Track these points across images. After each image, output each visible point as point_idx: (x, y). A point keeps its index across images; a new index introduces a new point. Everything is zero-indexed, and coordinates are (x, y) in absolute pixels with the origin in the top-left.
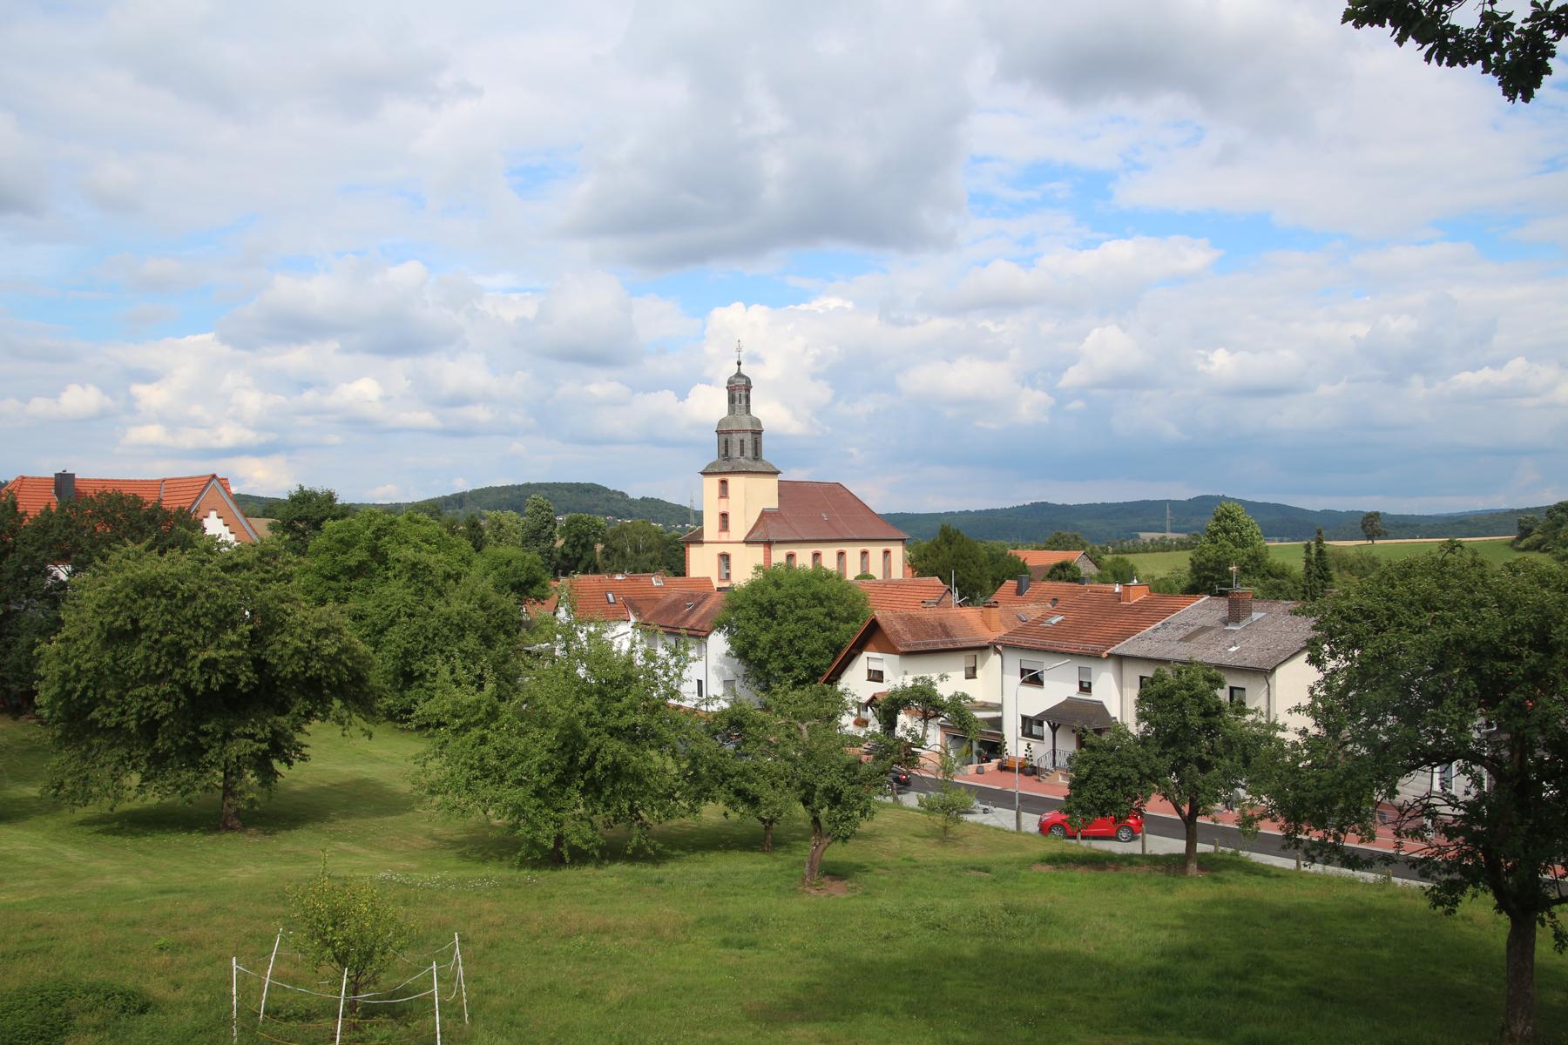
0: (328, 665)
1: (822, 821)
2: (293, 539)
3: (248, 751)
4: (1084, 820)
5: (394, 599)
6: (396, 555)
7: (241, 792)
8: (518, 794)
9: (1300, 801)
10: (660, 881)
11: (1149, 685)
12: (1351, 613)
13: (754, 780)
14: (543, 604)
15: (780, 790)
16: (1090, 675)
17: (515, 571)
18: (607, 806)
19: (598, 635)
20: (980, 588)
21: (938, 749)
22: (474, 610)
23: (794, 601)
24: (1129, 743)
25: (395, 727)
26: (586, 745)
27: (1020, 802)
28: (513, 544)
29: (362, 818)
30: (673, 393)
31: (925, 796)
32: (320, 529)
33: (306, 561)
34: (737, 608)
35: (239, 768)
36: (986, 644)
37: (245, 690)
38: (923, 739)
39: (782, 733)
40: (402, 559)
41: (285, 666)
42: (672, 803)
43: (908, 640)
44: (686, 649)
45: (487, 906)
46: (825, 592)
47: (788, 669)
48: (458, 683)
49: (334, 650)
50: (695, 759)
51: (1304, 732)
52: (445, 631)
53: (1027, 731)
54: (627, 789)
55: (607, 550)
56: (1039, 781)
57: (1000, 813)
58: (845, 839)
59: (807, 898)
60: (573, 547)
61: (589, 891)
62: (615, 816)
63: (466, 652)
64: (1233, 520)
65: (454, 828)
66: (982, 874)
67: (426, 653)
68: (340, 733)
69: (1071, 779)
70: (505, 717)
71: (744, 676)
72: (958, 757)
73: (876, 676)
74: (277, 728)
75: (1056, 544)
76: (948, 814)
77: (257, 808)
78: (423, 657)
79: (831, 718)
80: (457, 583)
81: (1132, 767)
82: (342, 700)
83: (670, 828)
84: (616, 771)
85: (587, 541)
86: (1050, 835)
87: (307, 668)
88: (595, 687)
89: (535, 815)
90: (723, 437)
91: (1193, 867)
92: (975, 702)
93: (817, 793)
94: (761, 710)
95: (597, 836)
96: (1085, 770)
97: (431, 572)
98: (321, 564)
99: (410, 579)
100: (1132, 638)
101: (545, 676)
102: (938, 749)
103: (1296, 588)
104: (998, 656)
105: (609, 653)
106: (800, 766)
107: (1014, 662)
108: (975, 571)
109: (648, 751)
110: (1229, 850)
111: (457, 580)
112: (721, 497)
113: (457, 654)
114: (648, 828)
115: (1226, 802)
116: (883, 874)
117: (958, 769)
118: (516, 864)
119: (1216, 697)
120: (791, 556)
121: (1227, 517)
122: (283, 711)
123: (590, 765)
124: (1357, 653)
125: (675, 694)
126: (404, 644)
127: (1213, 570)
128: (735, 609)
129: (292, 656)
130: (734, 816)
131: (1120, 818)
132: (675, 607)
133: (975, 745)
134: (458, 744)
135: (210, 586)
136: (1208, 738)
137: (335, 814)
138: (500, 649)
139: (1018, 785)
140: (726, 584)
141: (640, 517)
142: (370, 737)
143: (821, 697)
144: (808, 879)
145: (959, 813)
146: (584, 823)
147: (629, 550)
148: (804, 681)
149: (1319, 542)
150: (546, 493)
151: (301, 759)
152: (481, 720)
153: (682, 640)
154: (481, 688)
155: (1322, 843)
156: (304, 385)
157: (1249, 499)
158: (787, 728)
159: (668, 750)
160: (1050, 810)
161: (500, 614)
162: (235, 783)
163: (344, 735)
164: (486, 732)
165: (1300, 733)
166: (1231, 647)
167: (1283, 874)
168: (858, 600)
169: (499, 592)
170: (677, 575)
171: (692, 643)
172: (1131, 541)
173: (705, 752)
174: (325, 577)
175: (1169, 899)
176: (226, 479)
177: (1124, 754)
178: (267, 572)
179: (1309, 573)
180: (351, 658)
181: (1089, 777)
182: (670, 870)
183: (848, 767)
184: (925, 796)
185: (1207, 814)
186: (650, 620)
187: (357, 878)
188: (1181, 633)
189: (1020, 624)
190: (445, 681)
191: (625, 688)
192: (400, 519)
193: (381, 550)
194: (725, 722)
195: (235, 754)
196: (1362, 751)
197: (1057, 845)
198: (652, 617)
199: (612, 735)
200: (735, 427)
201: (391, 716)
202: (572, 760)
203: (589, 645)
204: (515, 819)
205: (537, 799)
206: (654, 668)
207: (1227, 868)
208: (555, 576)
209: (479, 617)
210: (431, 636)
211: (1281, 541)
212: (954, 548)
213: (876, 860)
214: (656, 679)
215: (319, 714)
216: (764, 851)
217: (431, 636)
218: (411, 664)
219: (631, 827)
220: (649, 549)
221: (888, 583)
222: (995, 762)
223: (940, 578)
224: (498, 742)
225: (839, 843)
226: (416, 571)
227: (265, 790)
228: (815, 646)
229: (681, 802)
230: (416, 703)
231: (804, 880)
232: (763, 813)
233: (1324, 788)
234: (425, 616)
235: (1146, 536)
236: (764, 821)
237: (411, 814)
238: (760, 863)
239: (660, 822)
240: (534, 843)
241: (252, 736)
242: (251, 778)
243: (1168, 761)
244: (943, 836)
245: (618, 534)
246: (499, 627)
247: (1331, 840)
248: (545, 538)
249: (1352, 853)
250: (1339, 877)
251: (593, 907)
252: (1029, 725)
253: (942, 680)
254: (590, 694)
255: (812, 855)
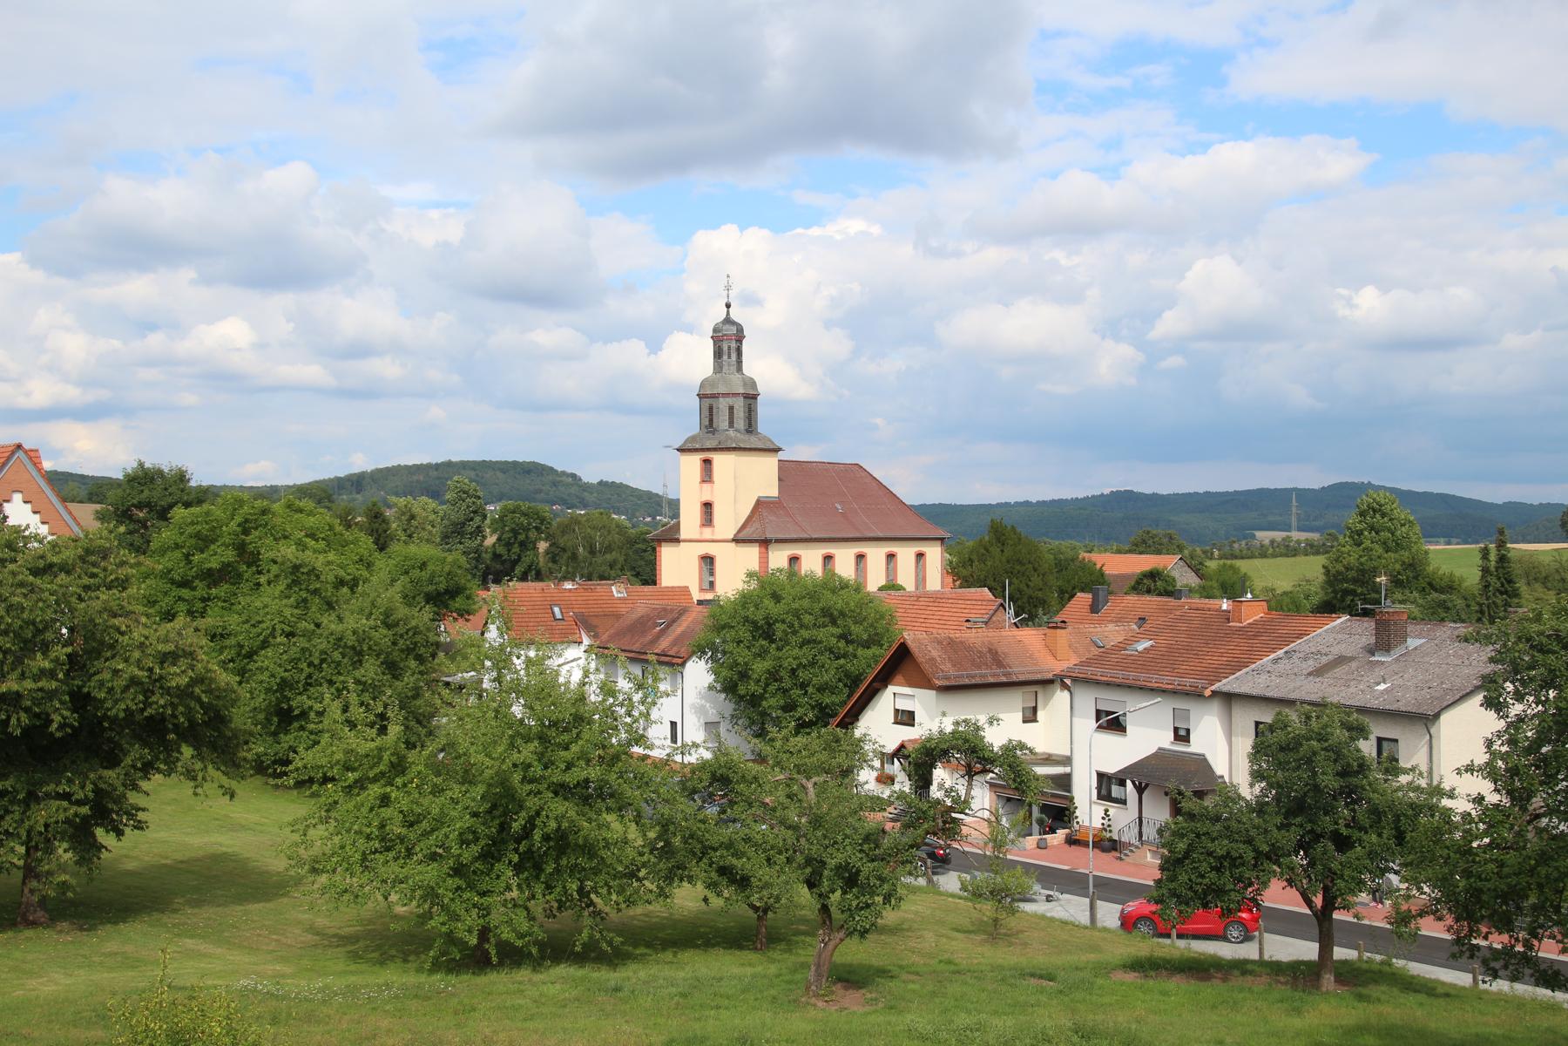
0: (176, 700)
1: (833, 909)
2: (130, 533)
3: (62, 817)
4: (1181, 912)
5: (267, 613)
6: (271, 555)
7: (50, 873)
8: (430, 873)
9: (1475, 893)
10: (617, 989)
11: (1268, 733)
12: (1544, 640)
13: (743, 854)
14: (467, 620)
15: (777, 868)
16: (1188, 719)
17: (432, 576)
18: (549, 887)
19: (540, 661)
20: (1043, 603)
21: (986, 814)
22: (375, 628)
23: (799, 618)
24: (1240, 810)
25: (267, 783)
26: (521, 807)
27: (1094, 886)
28: (428, 541)
29: (219, 906)
30: (642, 344)
31: (968, 878)
32: (167, 519)
33: (148, 562)
34: (723, 627)
35: (48, 840)
36: (1050, 676)
37: (58, 735)
38: (966, 802)
39: (781, 793)
40: (279, 560)
41: (116, 702)
42: (635, 884)
43: (948, 671)
44: (656, 680)
45: (385, 1023)
46: (839, 606)
47: (789, 707)
48: (352, 725)
49: (184, 680)
50: (665, 826)
51: (1479, 799)
52: (337, 656)
53: (1104, 792)
54: (576, 865)
55: (553, 549)
56: (1121, 859)
57: (1069, 901)
58: (863, 933)
59: (812, 1013)
60: (509, 545)
61: (521, 1002)
62: (560, 902)
63: (364, 683)
64: (1383, 515)
65: (345, 918)
66: (1045, 983)
67: (310, 685)
68: (190, 792)
69: (1162, 857)
70: (415, 769)
71: (732, 716)
72: (1013, 825)
73: (905, 718)
74: (103, 786)
75: (1143, 545)
76: (1000, 902)
77: (70, 895)
78: (305, 690)
79: (847, 772)
80: (353, 592)
81: (1244, 842)
82: (193, 746)
83: (633, 918)
84: (561, 841)
85: (527, 537)
86: (1135, 932)
87: (147, 704)
88: (534, 730)
89: (452, 900)
90: (707, 402)
91: (1328, 980)
92: (1035, 754)
93: (826, 873)
94: (754, 761)
95: (535, 929)
96: (1182, 846)
97: (318, 577)
98: (169, 565)
99: (289, 587)
100: (1245, 670)
101: (468, 715)
102: (986, 814)
103: (1468, 606)
104: (1066, 694)
105: (554, 684)
106: (805, 836)
107: (1087, 701)
108: (1036, 580)
109: (604, 815)
110: (1378, 958)
111: (353, 588)
112: (703, 481)
113: (352, 686)
114: (602, 919)
115: (1373, 892)
116: (913, 982)
117: (1013, 842)
118: (427, 966)
119: (1358, 750)
120: (794, 560)
121: (1374, 511)
122: (112, 761)
123: (527, 833)
124: (1552, 694)
125: (640, 739)
126: (281, 673)
127: (1355, 581)
128: (720, 628)
129: (127, 688)
130: (717, 902)
131: (1230, 911)
132: (642, 625)
133: (1035, 810)
134: (350, 805)
135: (13, 594)
136: (1347, 805)
137: (181, 901)
138: (409, 679)
139: (1093, 864)
140: (709, 596)
141: (597, 506)
142: (232, 796)
143: (832, 746)
144: (813, 988)
145: (1013, 900)
146: (518, 911)
147: (581, 549)
148: (811, 724)
149: (1501, 545)
150: (472, 474)
151: (135, 827)
152: (383, 774)
153: (650, 669)
154: (383, 730)
155: (1507, 952)
156: (146, 326)
157: (1404, 487)
158: (788, 785)
159: (630, 814)
160: (1134, 898)
161: (411, 633)
162: (41, 860)
163: (196, 794)
164: (388, 789)
165: (1474, 801)
166: (1378, 684)
167: (1452, 992)
168: (882, 617)
169: (410, 605)
170: (645, 583)
171: (663, 672)
172: (1243, 543)
173: (680, 816)
174: (173, 582)
175: (1297, 1022)
176: (37, 451)
177: (1234, 824)
178: (93, 576)
179: (1486, 587)
180: (209, 691)
181: (1187, 854)
182: (631, 974)
183: (867, 839)
184: (968, 878)
185: (1346, 907)
186: (608, 641)
187: (208, 988)
188: (1311, 665)
189: (1096, 651)
190: (335, 722)
191: (575, 731)
192: (276, 507)
193: (251, 547)
194: (706, 777)
195: (42, 822)
196: (1561, 827)
197: (1144, 945)
198: (612, 638)
199: (556, 793)
200: (722, 390)
201: (260, 768)
202: (503, 827)
203: (528, 675)
204: (426, 906)
205: (457, 879)
206: (612, 705)
207: (1376, 982)
208: (484, 585)
209: (383, 637)
210: (316, 662)
211: (1449, 543)
212: (1008, 552)
213: (904, 963)
214: (616, 720)
215: (162, 766)
216: (756, 949)
217: (316, 662)
218: (289, 699)
219: (580, 916)
220: (609, 549)
221: (922, 596)
222: (1061, 834)
223: (990, 589)
224: (405, 804)
225: (856, 937)
226: (297, 575)
227: (84, 869)
228: (826, 678)
229: (646, 882)
230: (295, 752)
231: (808, 988)
232: (755, 899)
233: (1508, 876)
234: (308, 635)
235: (1264, 536)
236: (756, 909)
237: (285, 900)
238: (750, 965)
239: (619, 910)
240: (450, 938)
241: (66, 796)
242: (64, 853)
243: (1293, 835)
244: (993, 932)
245: (566, 529)
246: (408, 651)
247: (1519, 948)
248: (471, 534)
249: (1551, 967)
250: (1533, 1000)
251: (530, 1025)
252: (1106, 785)
253: (991, 723)
254: (528, 740)
255: (820, 956)
